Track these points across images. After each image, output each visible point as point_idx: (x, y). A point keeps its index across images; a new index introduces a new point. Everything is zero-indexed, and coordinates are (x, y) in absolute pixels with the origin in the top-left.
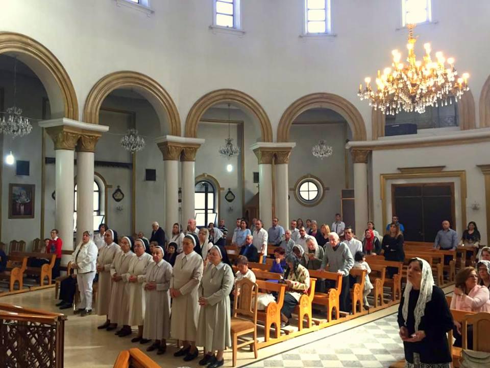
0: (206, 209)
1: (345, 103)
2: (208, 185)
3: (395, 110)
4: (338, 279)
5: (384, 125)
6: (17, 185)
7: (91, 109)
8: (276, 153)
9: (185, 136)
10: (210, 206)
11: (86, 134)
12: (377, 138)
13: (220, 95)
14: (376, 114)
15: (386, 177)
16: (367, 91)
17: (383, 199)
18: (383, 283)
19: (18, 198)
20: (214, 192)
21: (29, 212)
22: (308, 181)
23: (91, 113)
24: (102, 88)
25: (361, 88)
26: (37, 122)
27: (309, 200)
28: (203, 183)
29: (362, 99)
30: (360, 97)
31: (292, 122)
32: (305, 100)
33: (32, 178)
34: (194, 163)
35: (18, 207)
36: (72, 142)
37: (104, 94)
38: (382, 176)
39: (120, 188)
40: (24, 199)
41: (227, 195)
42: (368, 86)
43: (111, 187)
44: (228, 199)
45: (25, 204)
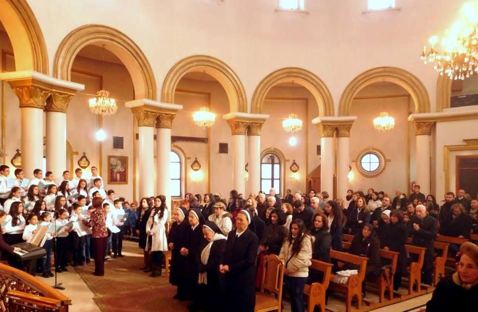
0: (273, 179)
1: (408, 75)
2: (274, 157)
3: (465, 73)
4: (393, 257)
5: (450, 96)
6: (113, 157)
7: (168, 91)
8: (338, 126)
9: (252, 112)
10: (277, 176)
11: (163, 112)
12: (442, 111)
13: (285, 73)
14: (367, 210)
15: (451, 149)
16: (432, 52)
17: (447, 171)
18: (444, 262)
19: (114, 167)
20: (280, 164)
21: (124, 179)
22: (370, 153)
23: (168, 94)
24: (177, 72)
25: (425, 50)
26: (124, 103)
27: (370, 171)
28: (270, 155)
29: (425, 63)
30: (423, 61)
31: (353, 97)
32: (367, 75)
33: (126, 151)
34: (259, 137)
35: (115, 175)
36: (40, 100)
37: (181, 74)
38: (446, 148)
39: (296, 162)
40: (119, 168)
41: (292, 166)
42: (433, 47)
43: (189, 158)
44: (293, 170)
45: (119, 172)
